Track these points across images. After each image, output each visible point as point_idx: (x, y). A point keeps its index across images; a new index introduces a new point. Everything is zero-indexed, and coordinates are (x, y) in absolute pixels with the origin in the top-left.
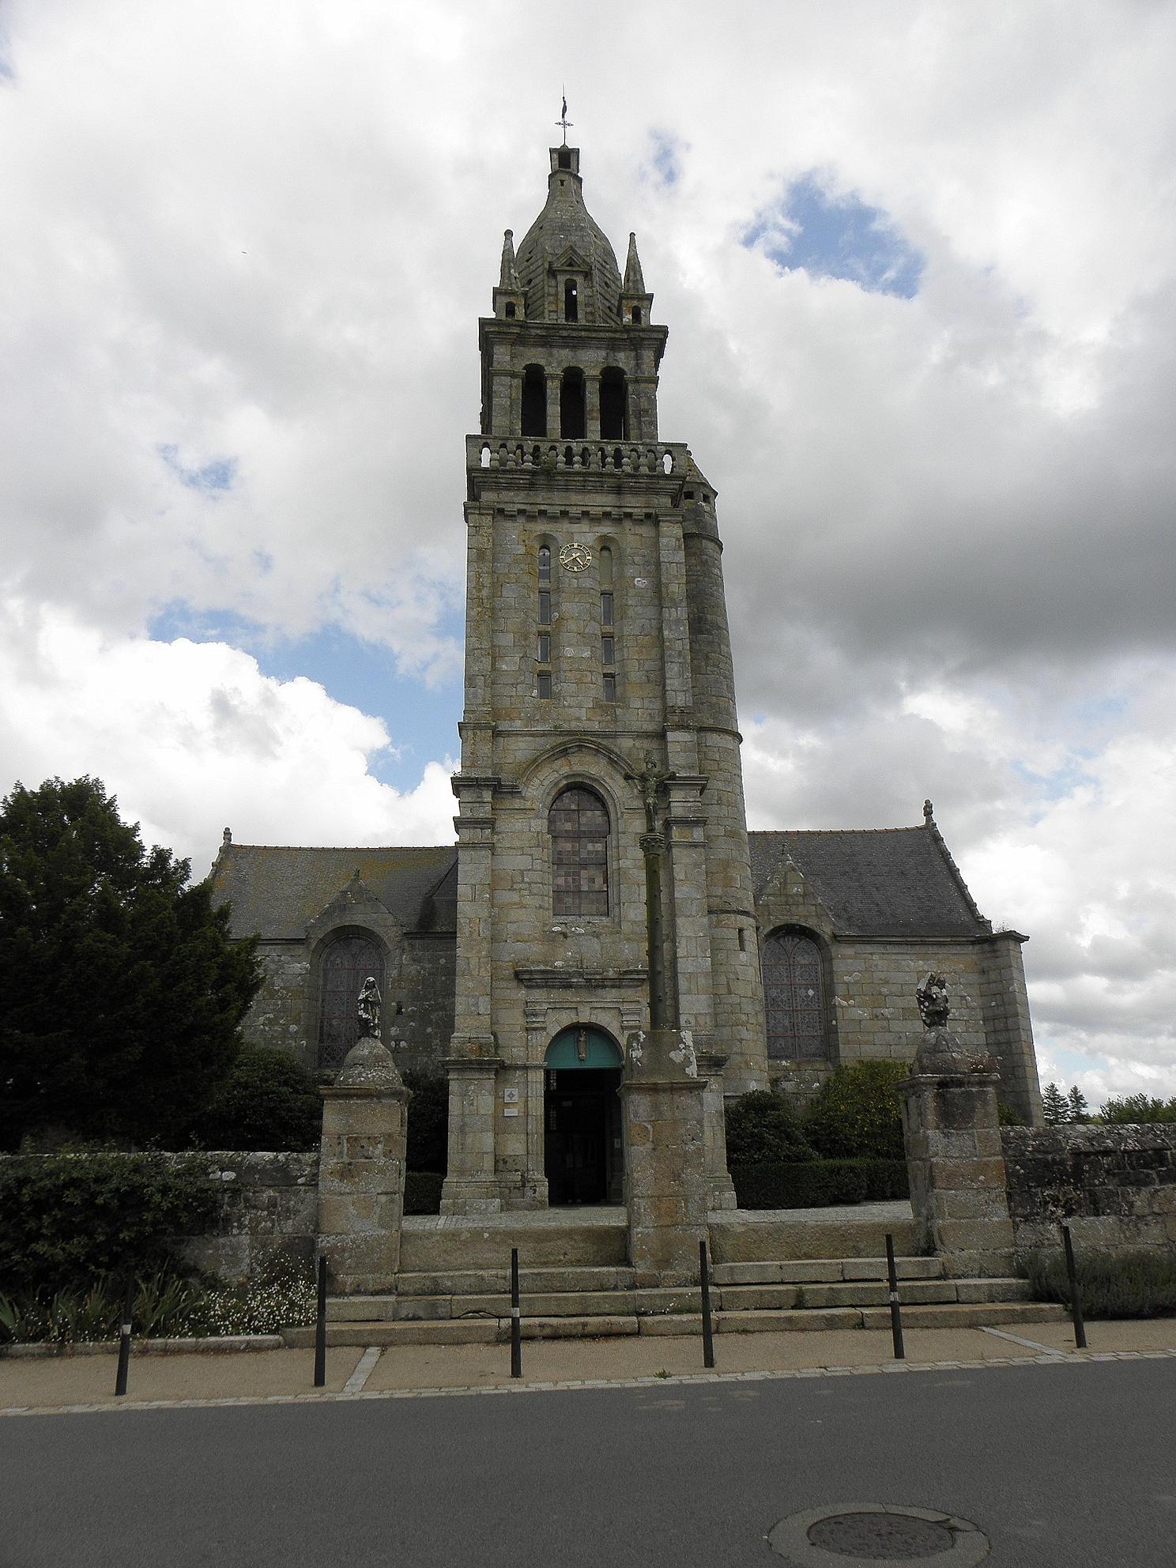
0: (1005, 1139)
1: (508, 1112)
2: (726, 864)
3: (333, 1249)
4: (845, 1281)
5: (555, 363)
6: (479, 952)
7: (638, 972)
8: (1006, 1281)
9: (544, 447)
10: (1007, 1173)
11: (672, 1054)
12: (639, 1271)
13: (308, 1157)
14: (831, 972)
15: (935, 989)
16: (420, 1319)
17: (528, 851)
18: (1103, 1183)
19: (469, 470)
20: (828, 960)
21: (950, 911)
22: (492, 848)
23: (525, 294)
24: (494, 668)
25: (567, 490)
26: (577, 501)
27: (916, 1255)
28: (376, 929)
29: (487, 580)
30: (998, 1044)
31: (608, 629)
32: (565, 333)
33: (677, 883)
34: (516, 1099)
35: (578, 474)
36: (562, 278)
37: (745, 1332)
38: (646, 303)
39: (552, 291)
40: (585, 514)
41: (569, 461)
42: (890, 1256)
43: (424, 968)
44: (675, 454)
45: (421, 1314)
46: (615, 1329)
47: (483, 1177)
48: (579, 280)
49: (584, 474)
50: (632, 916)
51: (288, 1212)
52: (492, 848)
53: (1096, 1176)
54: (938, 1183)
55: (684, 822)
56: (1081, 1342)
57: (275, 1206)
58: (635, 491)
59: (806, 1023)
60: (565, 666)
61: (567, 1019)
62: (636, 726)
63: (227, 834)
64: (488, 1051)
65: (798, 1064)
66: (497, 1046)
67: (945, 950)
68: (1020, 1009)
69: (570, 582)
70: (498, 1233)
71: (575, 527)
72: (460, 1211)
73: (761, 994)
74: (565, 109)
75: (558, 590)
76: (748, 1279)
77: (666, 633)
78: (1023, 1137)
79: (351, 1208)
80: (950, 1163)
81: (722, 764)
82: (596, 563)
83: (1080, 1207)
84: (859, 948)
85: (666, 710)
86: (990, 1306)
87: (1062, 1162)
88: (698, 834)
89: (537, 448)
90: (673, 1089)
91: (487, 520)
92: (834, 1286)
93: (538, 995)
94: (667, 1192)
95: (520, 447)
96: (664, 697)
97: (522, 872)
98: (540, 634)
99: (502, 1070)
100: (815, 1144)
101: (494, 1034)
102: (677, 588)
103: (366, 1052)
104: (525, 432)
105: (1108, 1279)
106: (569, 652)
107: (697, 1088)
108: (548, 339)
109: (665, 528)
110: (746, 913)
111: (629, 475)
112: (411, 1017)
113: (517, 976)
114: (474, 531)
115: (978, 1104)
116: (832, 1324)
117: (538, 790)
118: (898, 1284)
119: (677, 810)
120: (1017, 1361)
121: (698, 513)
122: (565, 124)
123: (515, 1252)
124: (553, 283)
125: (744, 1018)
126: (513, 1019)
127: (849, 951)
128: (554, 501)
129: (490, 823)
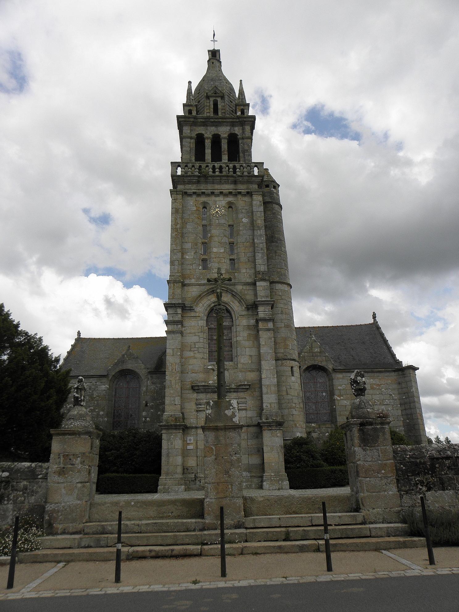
0: (395, 452)
1: (189, 447)
2: (285, 339)
3: (54, 511)
4: (312, 526)
5: (208, 132)
6: (176, 377)
7: (245, 385)
8: (396, 525)
9: (203, 166)
10: (396, 469)
11: (226, 412)
12: (207, 521)
13: (45, 465)
14: (333, 385)
15: (359, 378)
16: (91, 547)
17: (197, 334)
18: (446, 474)
19: (172, 176)
20: (331, 380)
21: (384, 358)
22: (182, 333)
23: (196, 106)
24: (182, 258)
25: (213, 183)
26: (218, 187)
27: (351, 512)
28: (137, 370)
29: (179, 221)
30: (407, 415)
31: (231, 240)
32: (212, 120)
34: (192, 441)
35: (218, 176)
36: (212, 99)
37: (256, 554)
38: (247, 107)
39: (208, 104)
40: (221, 193)
41: (214, 172)
43: (157, 387)
44: (259, 167)
45: (92, 544)
46: (188, 552)
47: (177, 476)
48: (219, 100)
49: (220, 176)
50: (242, 361)
51: (33, 493)
52: (182, 333)
53: (443, 470)
54: (361, 475)
55: (265, 320)
56: (432, 561)
57: (26, 489)
58: (242, 183)
59: (320, 407)
60: (213, 256)
62: (243, 280)
63: (79, 333)
64: (179, 421)
65: (319, 425)
66: (184, 418)
67: (382, 374)
68: (416, 399)
69: (215, 221)
70: (138, 502)
71: (217, 199)
72: (166, 491)
73: (301, 394)
74: (214, 35)
75: (210, 225)
76: (262, 525)
77: (256, 240)
78: (405, 451)
79: (63, 490)
80: (367, 464)
82: (226, 213)
83: (435, 486)
84: (344, 374)
85: (257, 273)
86: (388, 539)
87: (425, 463)
88: (270, 325)
89: (200, 166)
90: (226, 428)
91: (180, 197)
92: (305, 528)
93: (202, 396)
94: (222, 480)
95: (193, 166)
96: (255, 268)
97: (195, 343)
98: (203, 243)
99: (186, 429)
100: (326, 460)
101: (183, 413)
102: (260, 222)
103: (76, 413)
104: (196, 160)
105: (450, 524)
106: (215, 250)
107: (238, 428)
108: (206, 123)
109: (255, 197)
110: (294, 360)
111: (239, 176)
112: (152, 407)
113: (193, 388)
114: (174, 201)
115: (381, 434)
116: (302, 549)
117: (202, 308)
118: (329, 528)
119: (261, 315)
120: (394, 574)
121: (271, 193)
122: (214, 41)
123: (120, 513)
124: (208, 101)
125: (294, 405)
126: (191, 407)
127: (340, 376)
128: (207, 188)
129: (181, 323)
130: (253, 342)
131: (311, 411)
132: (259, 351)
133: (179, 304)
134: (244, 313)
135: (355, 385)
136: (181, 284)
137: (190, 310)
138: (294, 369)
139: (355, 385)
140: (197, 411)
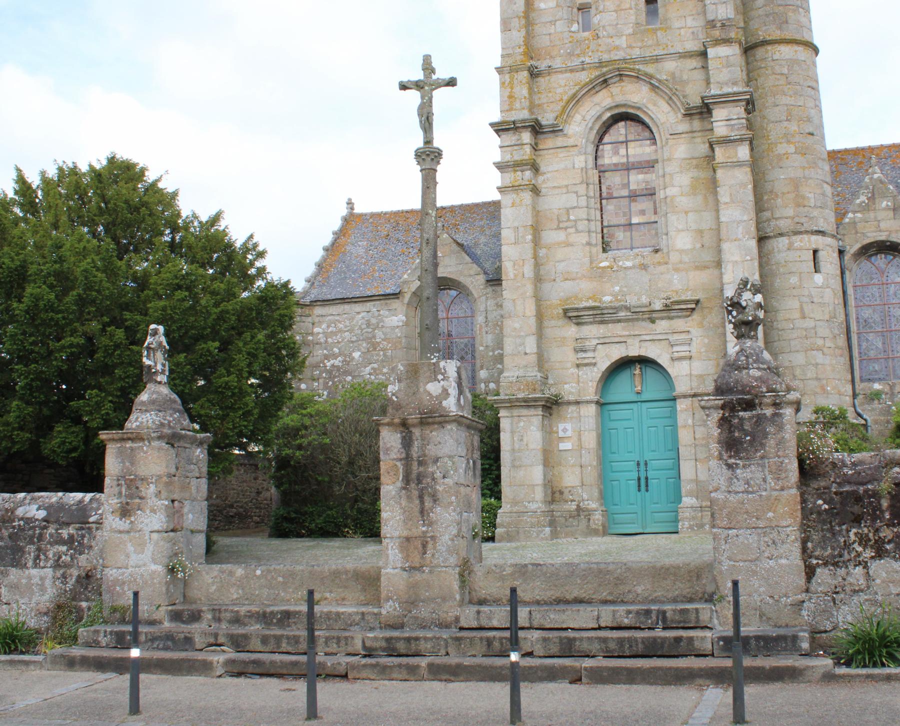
4: (600, 628)
22: (535, 191)
28: (461, 279)
33: (722, 207)
34: (569, 434)
42: (311, 613)
61: (617, 353)
63: (350, 203)
79: (129, 545)
81: (791, 78)
96: (704, 13)
97: (568, 210)
115: (770, 429)
117: (580, 126)
118: (521, 634)
119: (721, 130)
125: (820, 342)
130: (705, 197)
131: (872, 354)
132: (718, 218)
133: (524, 121)
134: (684, 127)
135: (734, 313)
136: (526, 74)
137: (554, 131)
138: (821, 254)
139: (734, 313)
140: (578, 366)
